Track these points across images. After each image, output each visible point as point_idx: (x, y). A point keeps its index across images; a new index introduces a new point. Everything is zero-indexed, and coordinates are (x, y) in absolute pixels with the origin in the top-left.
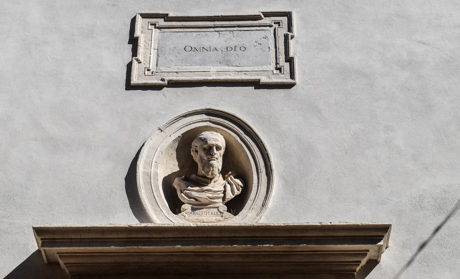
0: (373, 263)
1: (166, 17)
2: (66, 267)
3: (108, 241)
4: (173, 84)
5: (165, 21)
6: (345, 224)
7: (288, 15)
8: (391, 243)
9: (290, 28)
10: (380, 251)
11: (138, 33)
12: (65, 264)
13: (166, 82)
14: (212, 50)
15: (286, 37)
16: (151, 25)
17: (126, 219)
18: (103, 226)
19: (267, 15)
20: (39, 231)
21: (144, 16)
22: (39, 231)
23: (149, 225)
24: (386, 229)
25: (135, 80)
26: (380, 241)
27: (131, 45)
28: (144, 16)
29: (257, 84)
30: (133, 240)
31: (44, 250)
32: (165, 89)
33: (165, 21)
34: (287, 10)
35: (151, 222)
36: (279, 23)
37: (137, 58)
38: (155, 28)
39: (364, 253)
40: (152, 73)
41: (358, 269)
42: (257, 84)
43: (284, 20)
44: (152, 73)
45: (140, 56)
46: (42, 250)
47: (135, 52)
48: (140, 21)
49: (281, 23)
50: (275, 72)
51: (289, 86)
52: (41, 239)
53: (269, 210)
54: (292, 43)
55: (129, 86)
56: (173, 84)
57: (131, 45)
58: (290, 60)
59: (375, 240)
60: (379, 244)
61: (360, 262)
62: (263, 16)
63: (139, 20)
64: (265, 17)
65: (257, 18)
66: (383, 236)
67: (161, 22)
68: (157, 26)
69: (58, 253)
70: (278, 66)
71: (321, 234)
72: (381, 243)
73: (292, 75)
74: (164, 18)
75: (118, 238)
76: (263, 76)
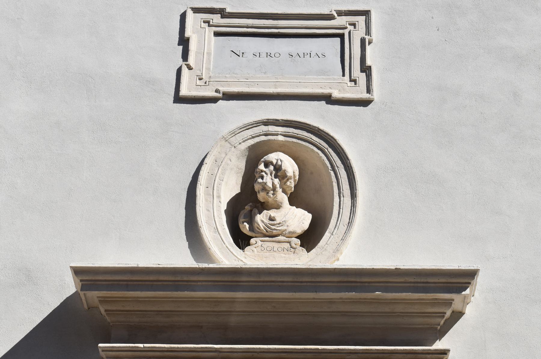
0: (458, 315)
1: (222, 13)
2: (107, 314)
3: (239, 285)
4: (229, 97)
5: (222, 17)
6: (158, 266)
7: (366, 13)
8: (476, 294)
9: (368, 31)
10: (465, 301)
11: (188, 34)
12: (106, 311)
13: (220, 95)
14: (312, 55)
15: (363, 41)
16: (204, 22)
17: (183, 259)
18: (365, 267)
19: (340, 13)
20: (77, 272)
21: (196, 10)
22: (77, 272)
23: (211, 266)
24: (472, 274)
25: (184, 92)
26: (465, 290)
27: (181, 47)
28: (196, 10)
29: (328, 99)
30: (147, 283)
31: (84, 294)
32: (220, 102)
33: (222, 17)
34: (366, 9)
35: (212, 262)
36: (354, 25)
37: (187, 63)
38: (209, 26)
39: (449, 303)
40: (205, 83)
41: (442, 322)
42: (328, 99)
43: (361, 20)
44: (205, 83)
45: (191, 60)
46: (82, 294)
47: (185, 56)
48: (190, 17)
49: (357, 26)
50: (349, 84)
51: (365, 103)
52: (81, 281)
53: (348, 249)
54: (368, 48)
55: (179, 99)
56: (229, 97)
57: (181, 47)
58: (366, 69)
59: (460, 288)
60: (463, 293)
61: (445, 313)
62: (336, 15)
63: (190, 15)
64: (338, 16)
65: (329, 17)
66: (470, 283)
67: (216, 19)
68: (211, 23)
69: (98, 297)
70: (353, 78)
71: (230, 278)
72: (468, 291)
73: (369, 90)
74: (221, 14)
75: (106, 281)
76: (335, 89)
